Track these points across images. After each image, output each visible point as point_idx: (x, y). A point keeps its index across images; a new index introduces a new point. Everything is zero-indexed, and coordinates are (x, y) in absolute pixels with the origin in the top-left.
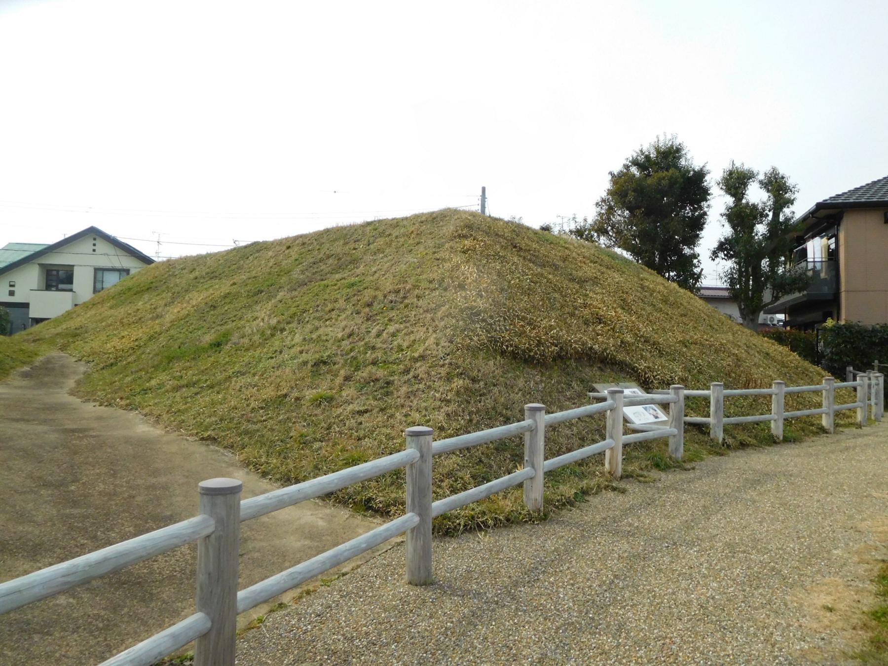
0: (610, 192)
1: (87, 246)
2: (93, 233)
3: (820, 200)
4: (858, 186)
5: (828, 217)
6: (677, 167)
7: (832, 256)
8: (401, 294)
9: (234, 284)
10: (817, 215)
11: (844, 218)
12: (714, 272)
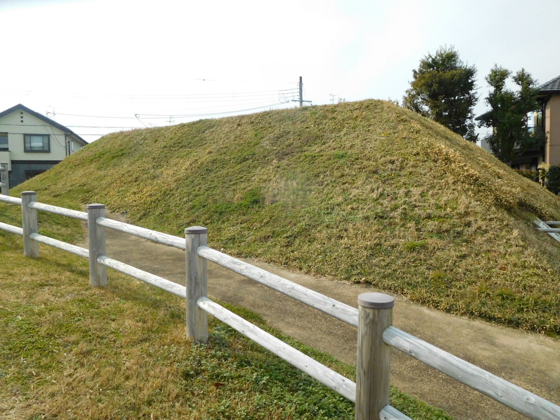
0: (413, 84)
1: (16, 118)
2: (20, 109)
6: (456, 68)
7: (541, 124)
8: (398, 163)
9: (210, 152)
11: (551, 101)
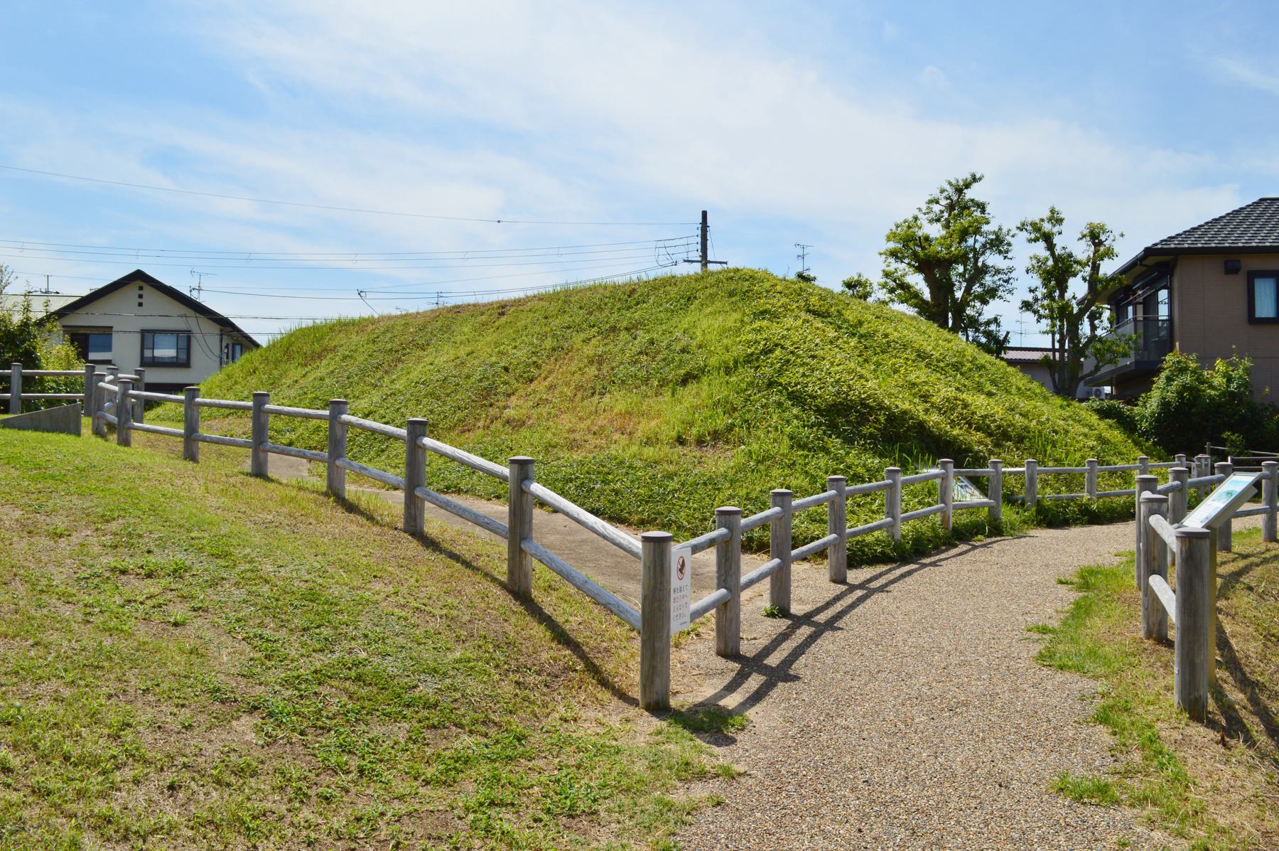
3: (1149, 245)
4: (1173, 234)
5: (1159, 265)
10: (1147, 262)
12: (1031, 334)
